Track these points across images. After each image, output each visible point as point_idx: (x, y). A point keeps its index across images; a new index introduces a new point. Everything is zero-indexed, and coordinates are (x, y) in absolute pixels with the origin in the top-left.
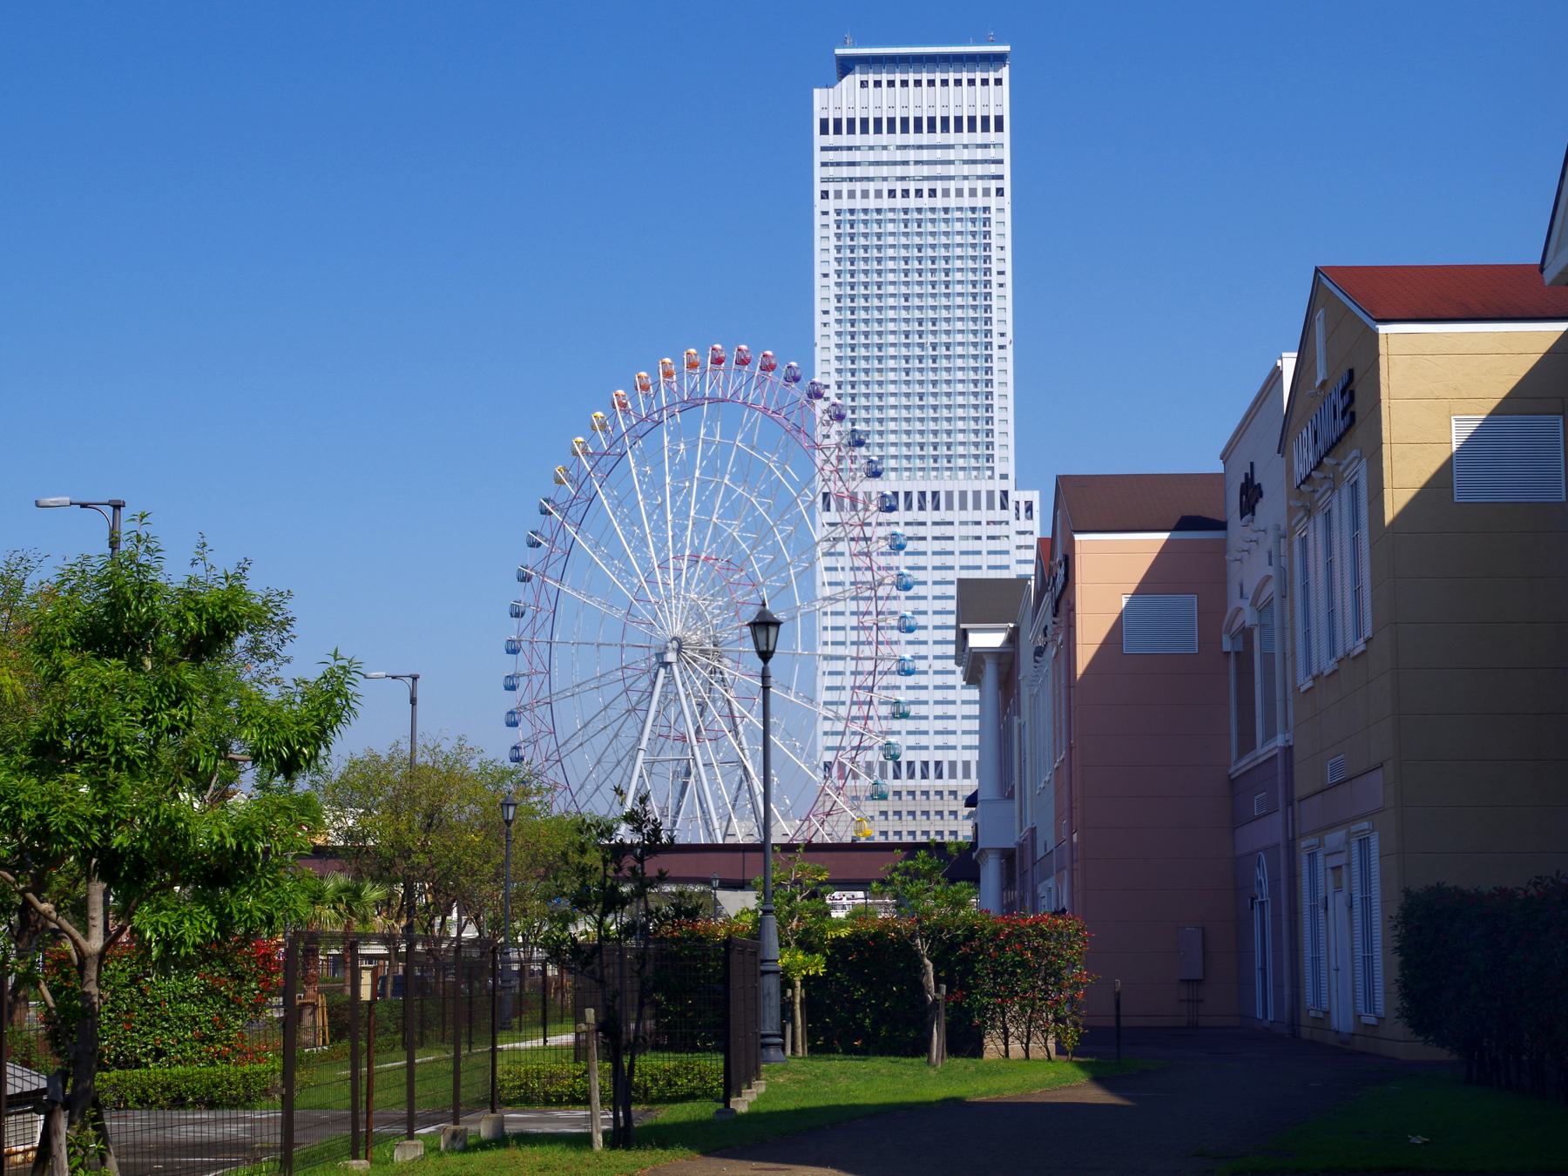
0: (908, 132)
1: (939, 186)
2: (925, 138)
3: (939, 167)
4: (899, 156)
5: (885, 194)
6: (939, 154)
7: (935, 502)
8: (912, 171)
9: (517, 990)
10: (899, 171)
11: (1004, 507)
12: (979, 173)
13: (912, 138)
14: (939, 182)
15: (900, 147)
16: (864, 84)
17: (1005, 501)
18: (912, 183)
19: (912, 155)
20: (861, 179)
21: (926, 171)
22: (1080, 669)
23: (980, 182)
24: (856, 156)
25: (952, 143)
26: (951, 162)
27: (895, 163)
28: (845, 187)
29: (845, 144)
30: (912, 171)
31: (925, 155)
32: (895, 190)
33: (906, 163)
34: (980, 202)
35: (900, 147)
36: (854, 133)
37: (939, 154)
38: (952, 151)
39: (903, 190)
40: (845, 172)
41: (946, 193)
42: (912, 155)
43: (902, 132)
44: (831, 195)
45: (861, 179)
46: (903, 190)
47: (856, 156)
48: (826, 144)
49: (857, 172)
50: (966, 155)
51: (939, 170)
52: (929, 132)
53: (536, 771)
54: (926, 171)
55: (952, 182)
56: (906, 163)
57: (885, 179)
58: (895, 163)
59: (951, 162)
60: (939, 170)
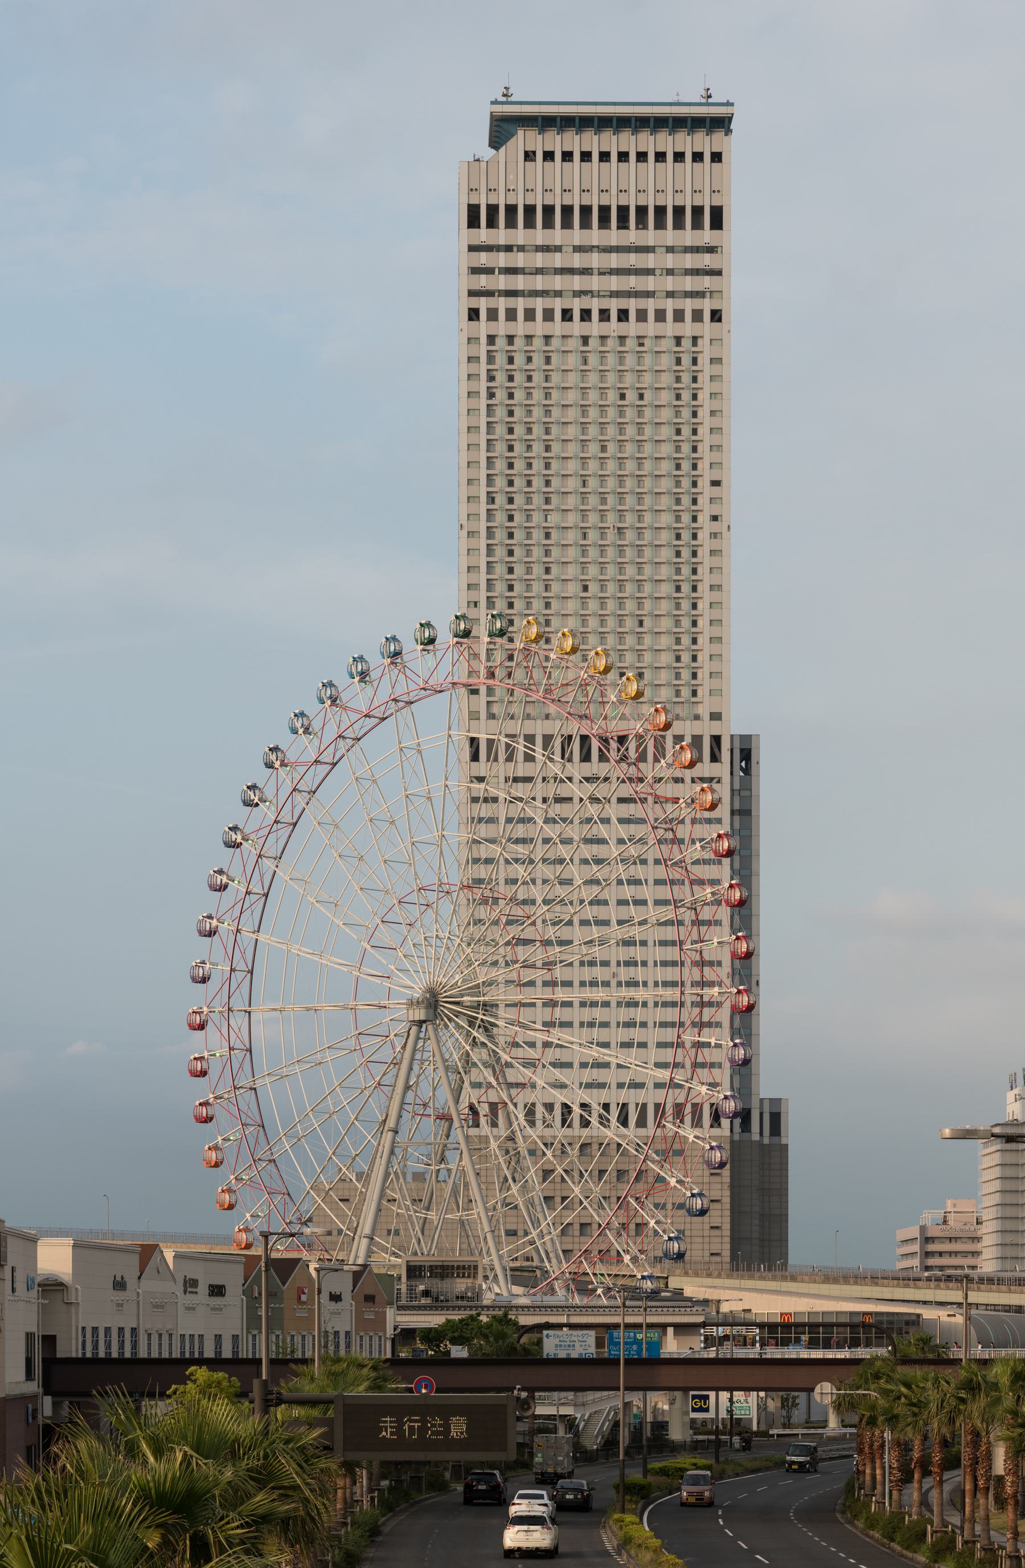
0: (609, 228)
1: (632, 305)
2: (614, 236)
3: (633, 278)
4: (577, 261)
5: (558, 315)
6: (632, 260)
7: (585, 750)
8: (595, 283)
9: (450, 1074)
10: (577, 282)
11: (715, 758)
12: (577, 287)
13: (595, 236)
14: (633, 300)
15: (578, 249)
16: (529, 156)
17: (716, 750)
18: (595, 300)
19: (595, 260)
20: (544, 293)
21: (614, 283)
22: (171, 1267)
23: (688, 301)
24: (650, 261)
25: (651, 243)
26: (649, 272)
27: (571, 271)
28: (502, 304)
29: (502, 242)
30: (595, 283)
31: (614, 260)
32: (608, 310)
33: (586, 271)
34: (688, 328)
35: (578, 249)
36: (627, 228)
37: (632, 260)
38: (651, 255)
39: (582, 310)
40: (502, 282)
41: (642, 315)
42: (595, 260)
43: (563, 227)
44: (632, 315)
45: (544, 293)
46: (582, 310)
47: (650, 261)
48: (476, 242)
49: (650, 283)
50: (670, 261)
51: (632, 282)
52: (618, 228)
53: (670, 817)
54: (614, 283)
55: (651, 300)
56: (586, 271)
57: (558, 294)
58: (571, 271)
59: (649, 272)
60: (632, 282)
